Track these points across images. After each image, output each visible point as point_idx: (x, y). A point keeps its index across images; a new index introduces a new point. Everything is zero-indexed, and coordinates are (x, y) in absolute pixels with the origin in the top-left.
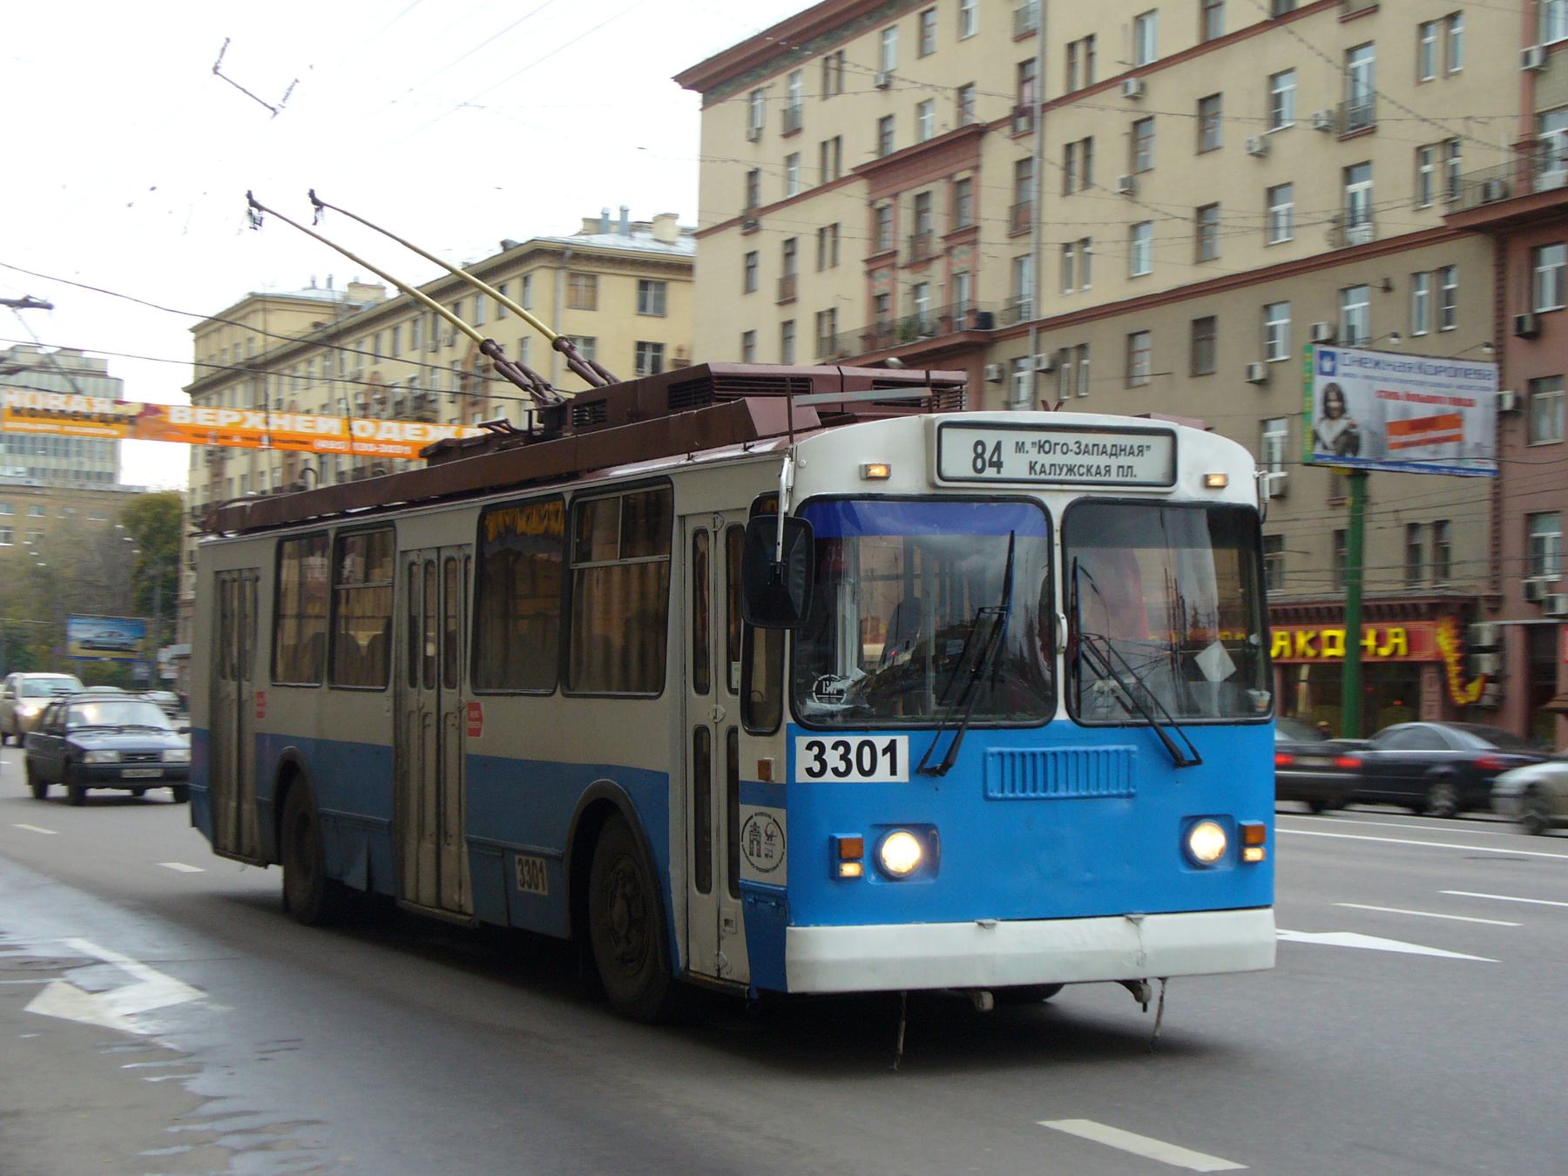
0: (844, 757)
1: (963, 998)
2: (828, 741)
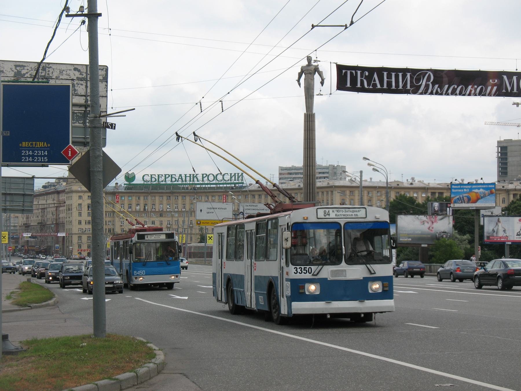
1: (324, 315)
2: (298, 267)
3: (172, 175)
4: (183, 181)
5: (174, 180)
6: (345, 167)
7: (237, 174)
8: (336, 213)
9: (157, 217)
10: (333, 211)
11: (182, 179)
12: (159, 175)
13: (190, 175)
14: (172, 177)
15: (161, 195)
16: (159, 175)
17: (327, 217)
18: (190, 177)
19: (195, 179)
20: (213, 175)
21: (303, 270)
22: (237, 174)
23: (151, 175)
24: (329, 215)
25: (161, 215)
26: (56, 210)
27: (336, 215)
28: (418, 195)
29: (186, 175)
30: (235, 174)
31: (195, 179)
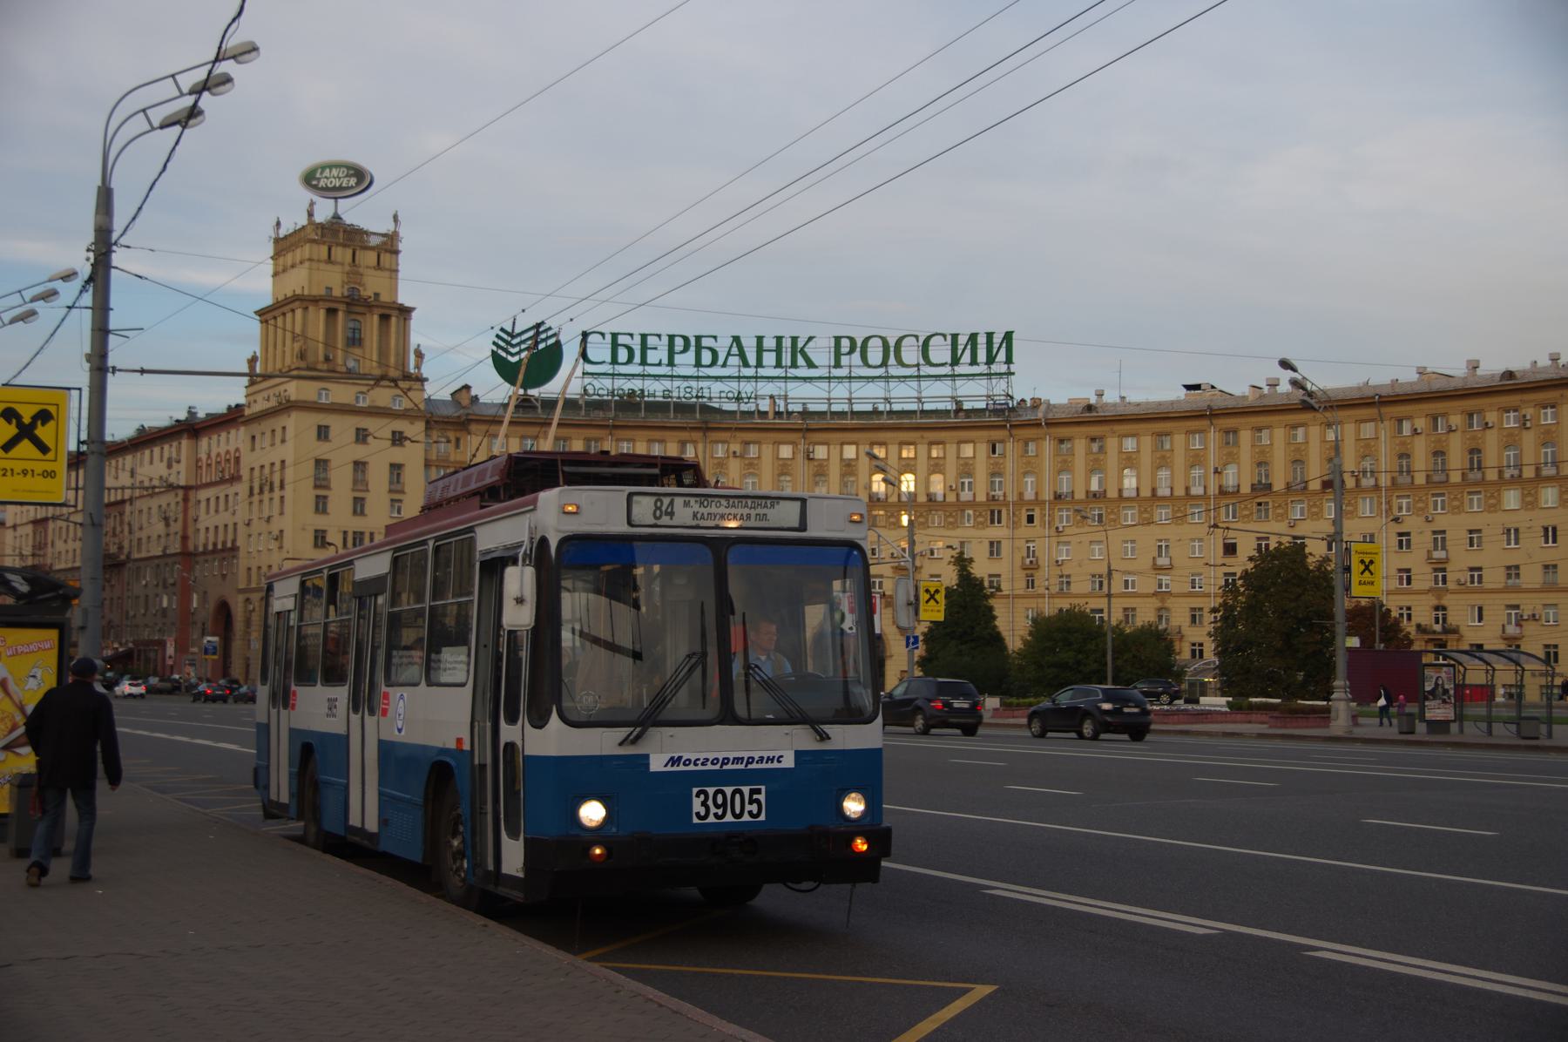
0: (704, 804)
3: (698, 338)
4: (746, 365)
5: (706, 357)
6: (467, 387)
7: (982, 340)
8: (696, 507)
9: (977, 526)
10: (686, 504)
11: (742, 355)
12: (644, 337)
13: (779, 339)
14: (699, 348)
15: (657, 434)
16: (644, 337)
17: (665, 520)
18: (778, 350)
19: (801, 361)
20: (884, 340)
21: (710, 802)
22: (982, 340)
23: (615, 336)
24: (671, 514)
25: (995, 518)
26: (186, 500)
27: (695, 515)
28: (1204, 442)
29: (760, 339)
30: (973, 338)
31: (801, 361)
